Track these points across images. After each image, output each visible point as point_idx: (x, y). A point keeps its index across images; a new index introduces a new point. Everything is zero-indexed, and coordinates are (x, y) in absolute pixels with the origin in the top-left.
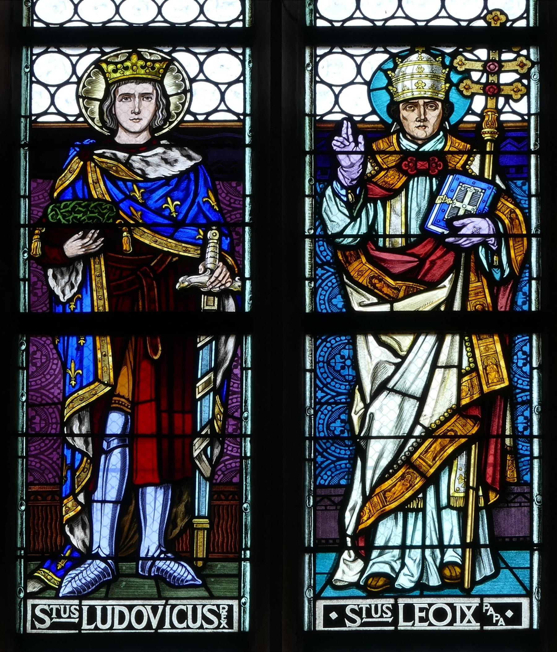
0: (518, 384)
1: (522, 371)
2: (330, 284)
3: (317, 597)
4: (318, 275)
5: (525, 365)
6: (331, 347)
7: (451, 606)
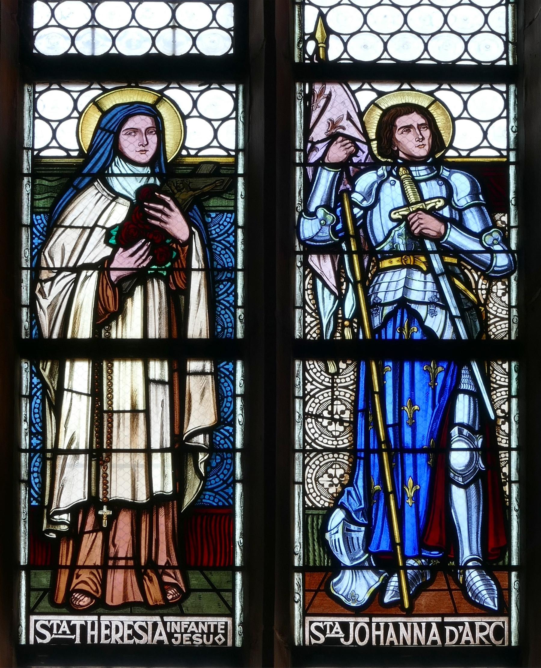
0: (497, 312)
1: (501, 300)
2: (317, 463)
5: (504, 294)
6: (320, 496)
7: (122, 622)
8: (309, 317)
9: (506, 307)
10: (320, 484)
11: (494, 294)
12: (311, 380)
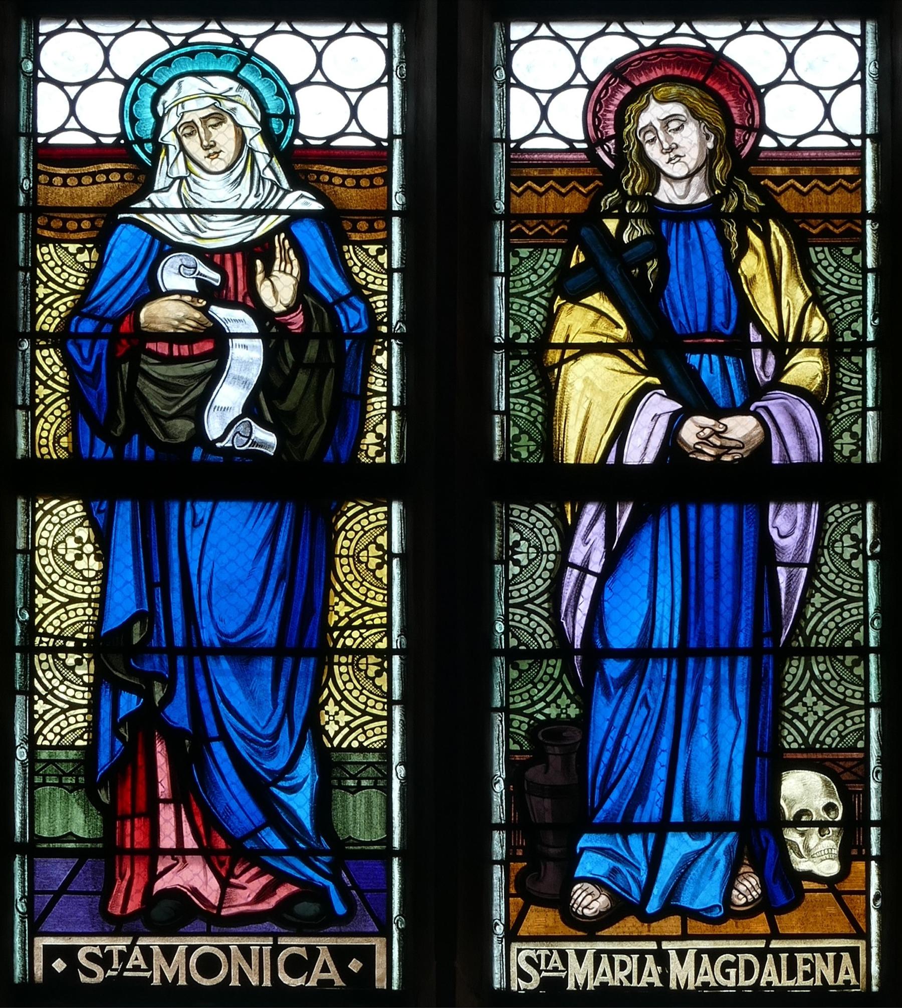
0: (367, 706)
1: (374, 685)
3: (35, 931)
6: (61, 267)
8: (40, 596)
9: (384, 374)
10: (61, 447)
11: (363, 565)
12: (45, 279)
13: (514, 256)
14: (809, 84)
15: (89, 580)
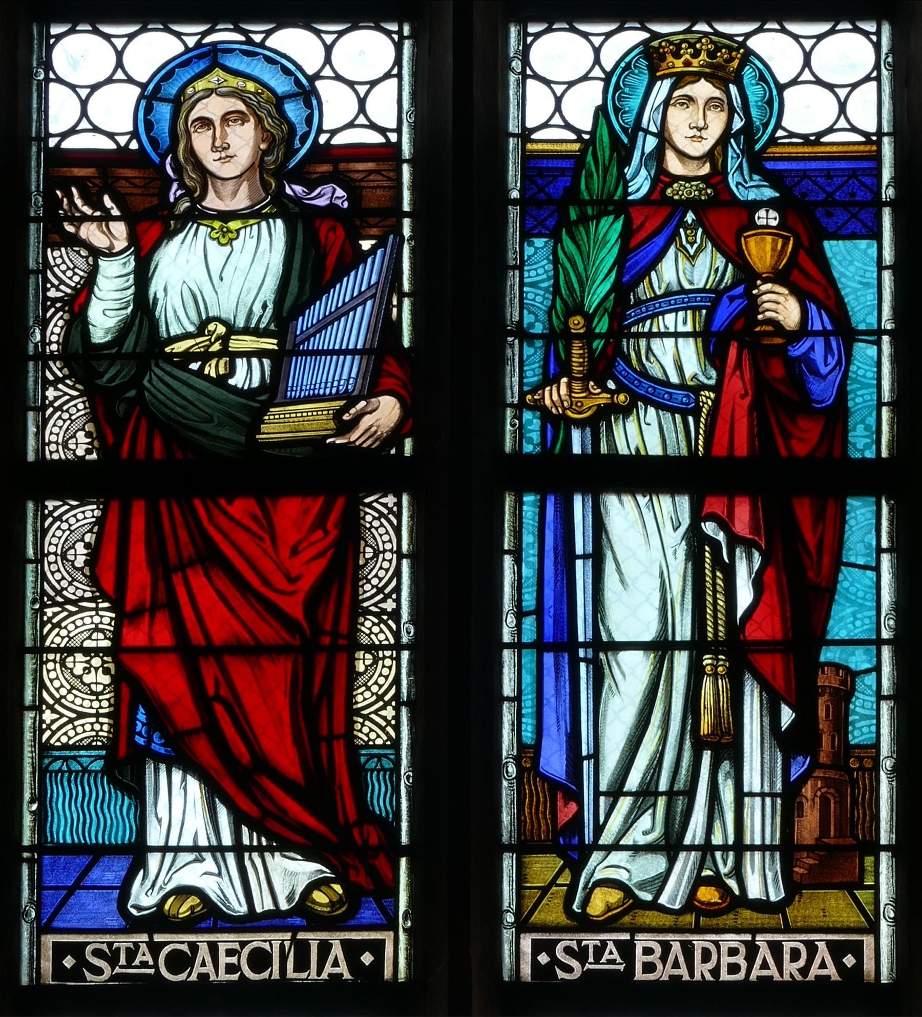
2: (70, 273)
4: (44, 722)
6: (73, 270)
7: (716, 943)
8: (48, 712)
12: (56, 282)
13: (529, 245)
14: (828, 82)
15: (97, 694)
